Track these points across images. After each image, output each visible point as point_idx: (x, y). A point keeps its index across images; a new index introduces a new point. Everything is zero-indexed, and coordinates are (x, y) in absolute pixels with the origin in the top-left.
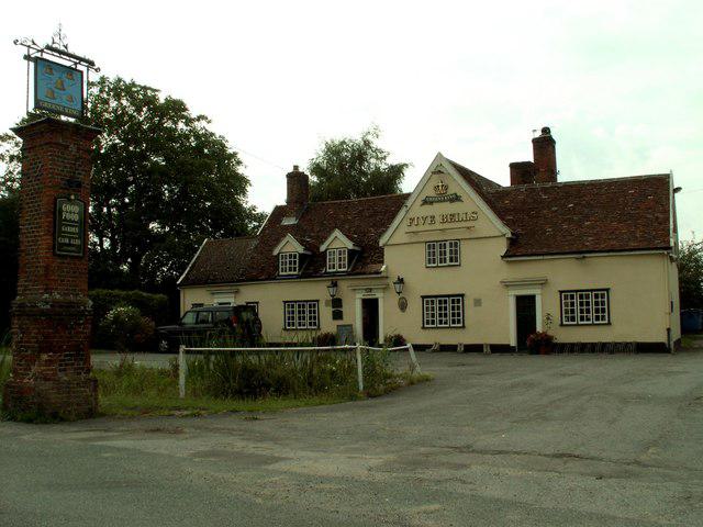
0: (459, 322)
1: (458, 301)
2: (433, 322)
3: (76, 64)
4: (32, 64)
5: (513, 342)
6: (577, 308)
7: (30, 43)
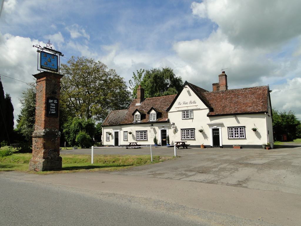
0: (193, 137)
1: (146, 132)
2: (185, 138)
3: (55, 53)
4: (39, 53)
5: (211, 145)
6: (234, 133)
7: (38, 46)
